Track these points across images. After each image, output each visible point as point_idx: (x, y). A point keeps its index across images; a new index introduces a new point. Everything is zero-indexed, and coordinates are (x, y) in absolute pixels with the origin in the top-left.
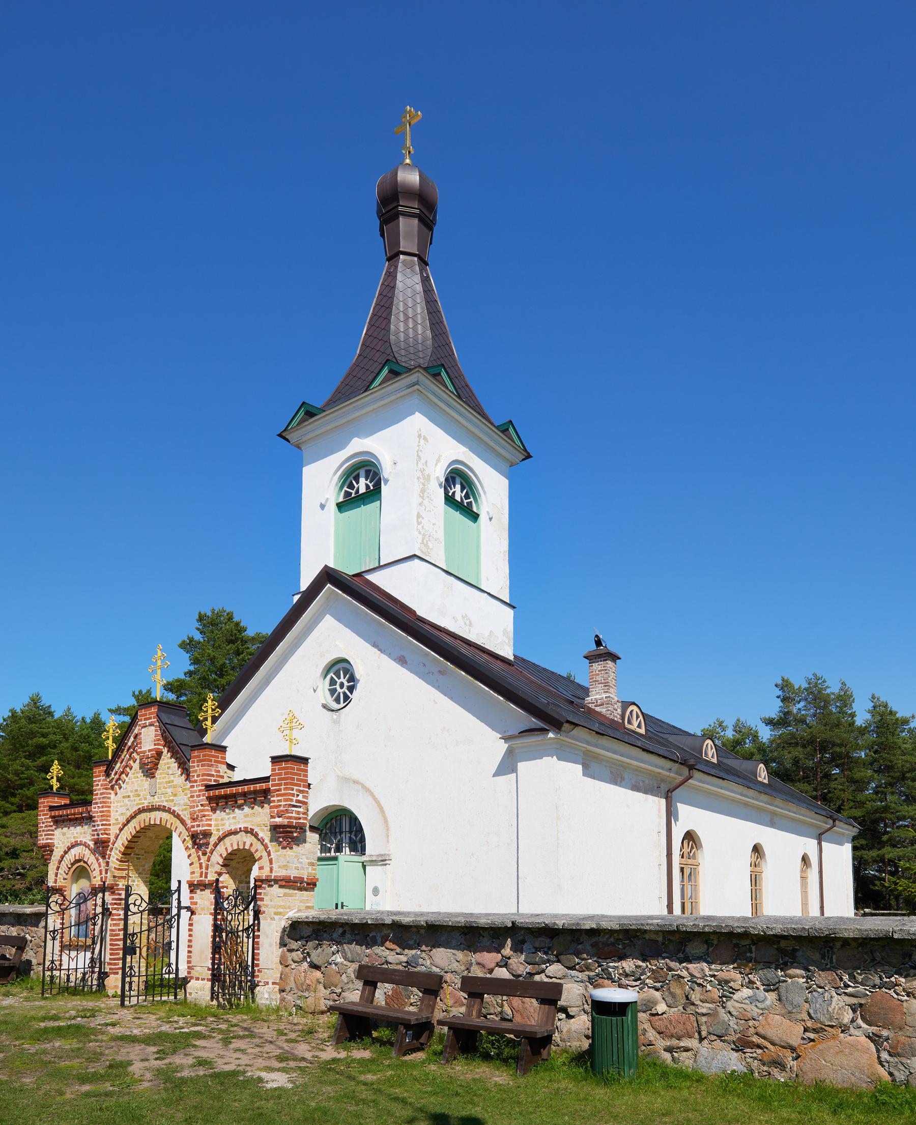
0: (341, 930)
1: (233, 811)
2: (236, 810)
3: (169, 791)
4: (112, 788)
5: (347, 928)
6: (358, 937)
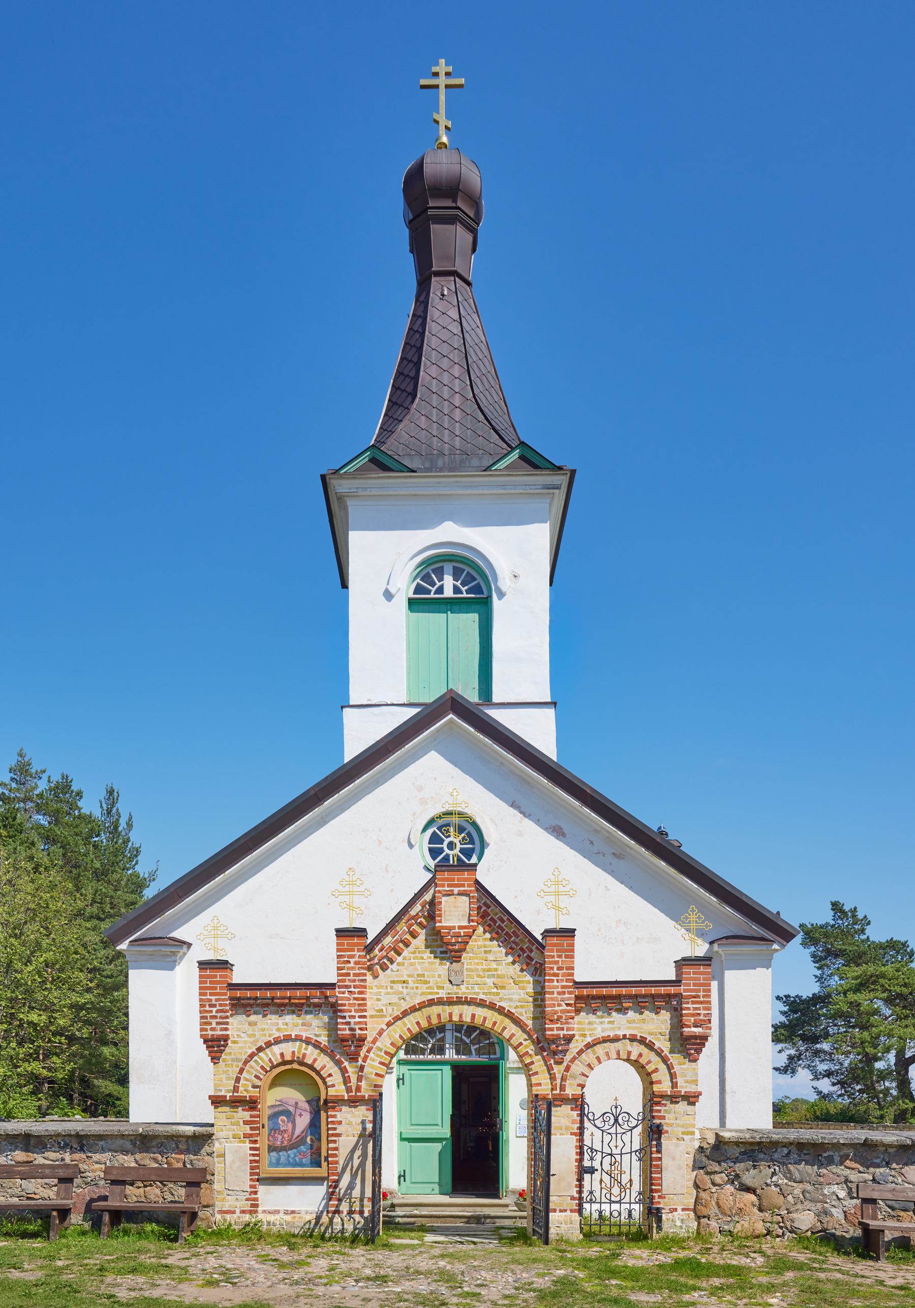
0: (785, 1151)
1: (609, 1014)
2: (614, 1014)
3: (490, 982)
4: (370, 968)
5: (793, 1149)
6: (807, 1157)
